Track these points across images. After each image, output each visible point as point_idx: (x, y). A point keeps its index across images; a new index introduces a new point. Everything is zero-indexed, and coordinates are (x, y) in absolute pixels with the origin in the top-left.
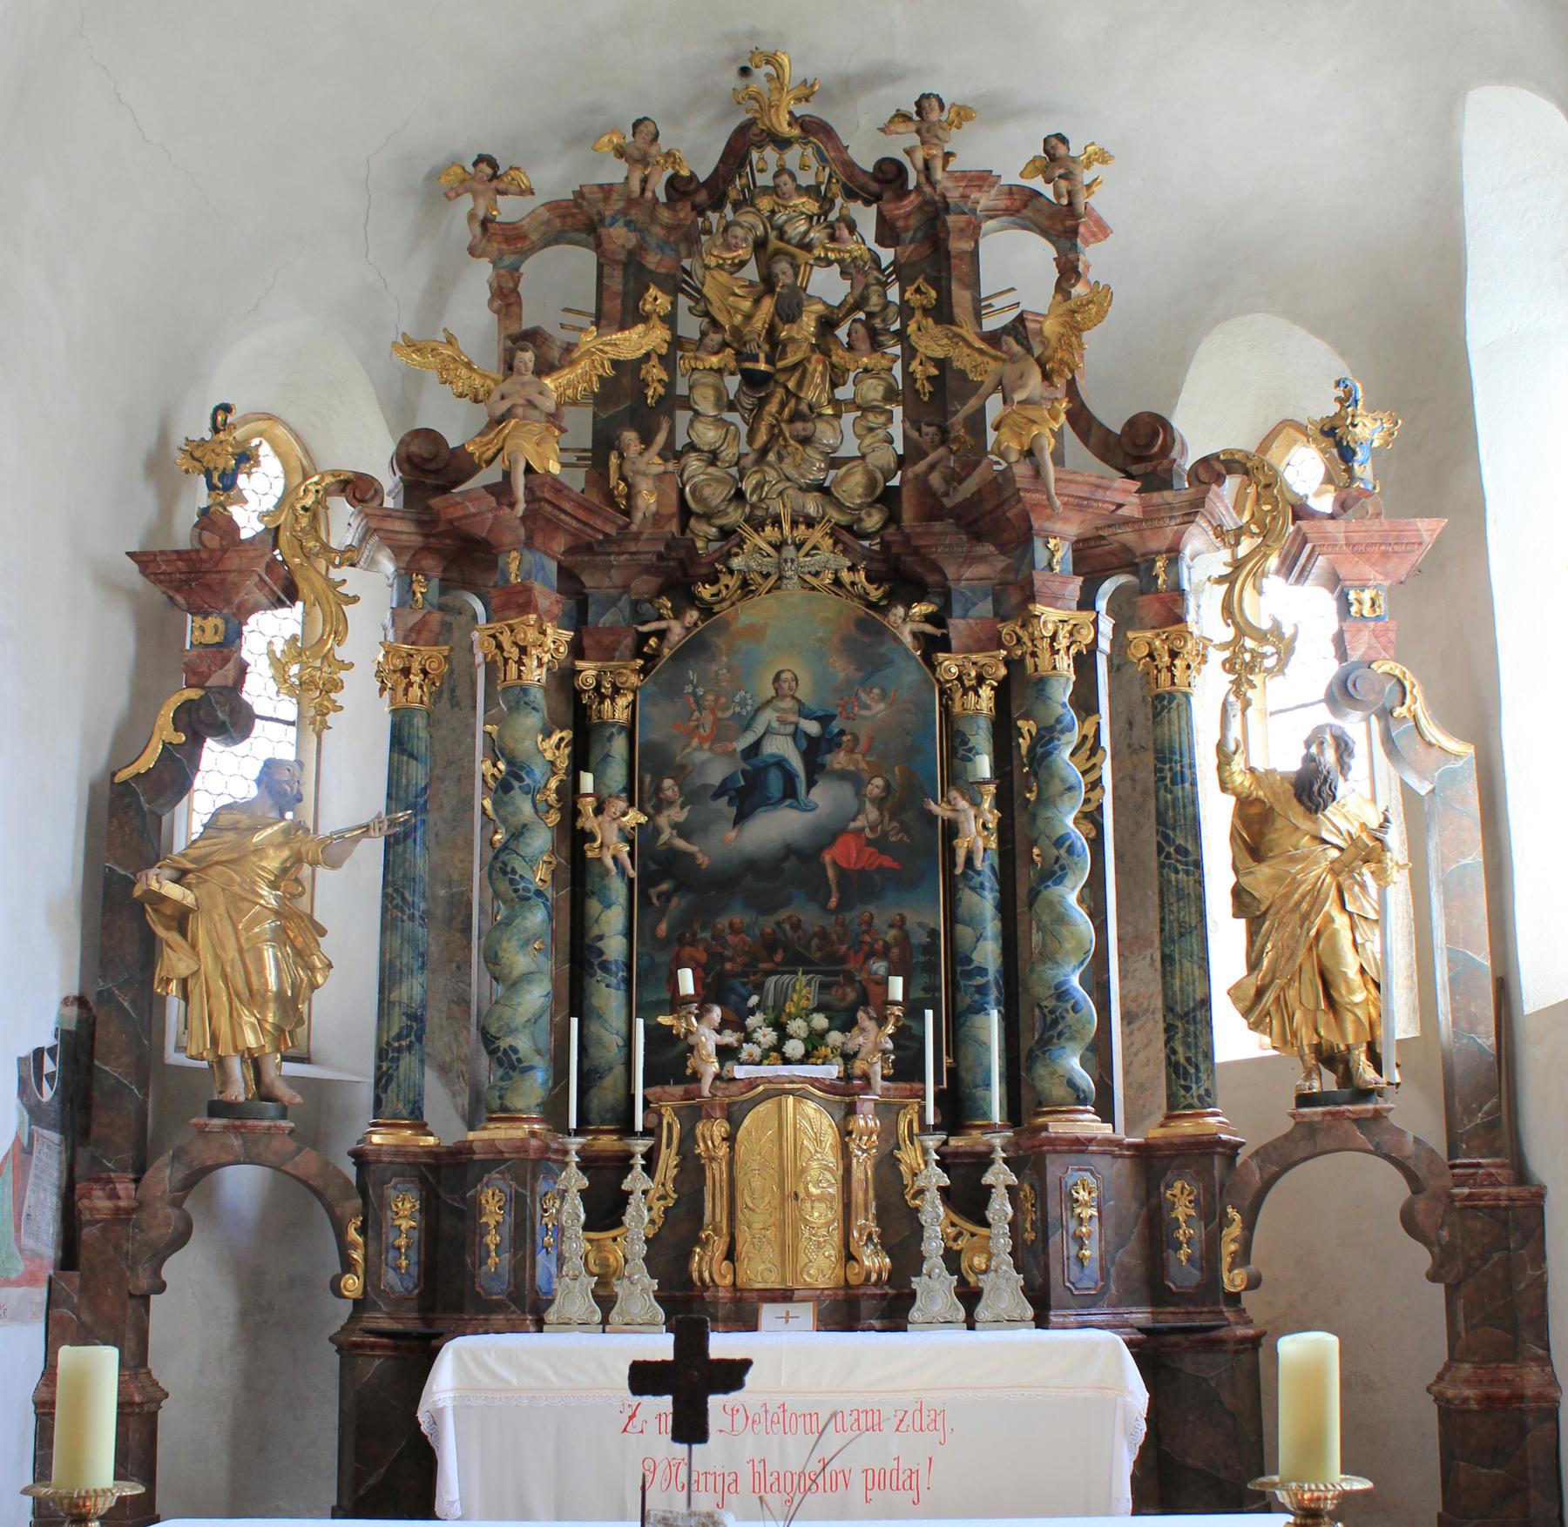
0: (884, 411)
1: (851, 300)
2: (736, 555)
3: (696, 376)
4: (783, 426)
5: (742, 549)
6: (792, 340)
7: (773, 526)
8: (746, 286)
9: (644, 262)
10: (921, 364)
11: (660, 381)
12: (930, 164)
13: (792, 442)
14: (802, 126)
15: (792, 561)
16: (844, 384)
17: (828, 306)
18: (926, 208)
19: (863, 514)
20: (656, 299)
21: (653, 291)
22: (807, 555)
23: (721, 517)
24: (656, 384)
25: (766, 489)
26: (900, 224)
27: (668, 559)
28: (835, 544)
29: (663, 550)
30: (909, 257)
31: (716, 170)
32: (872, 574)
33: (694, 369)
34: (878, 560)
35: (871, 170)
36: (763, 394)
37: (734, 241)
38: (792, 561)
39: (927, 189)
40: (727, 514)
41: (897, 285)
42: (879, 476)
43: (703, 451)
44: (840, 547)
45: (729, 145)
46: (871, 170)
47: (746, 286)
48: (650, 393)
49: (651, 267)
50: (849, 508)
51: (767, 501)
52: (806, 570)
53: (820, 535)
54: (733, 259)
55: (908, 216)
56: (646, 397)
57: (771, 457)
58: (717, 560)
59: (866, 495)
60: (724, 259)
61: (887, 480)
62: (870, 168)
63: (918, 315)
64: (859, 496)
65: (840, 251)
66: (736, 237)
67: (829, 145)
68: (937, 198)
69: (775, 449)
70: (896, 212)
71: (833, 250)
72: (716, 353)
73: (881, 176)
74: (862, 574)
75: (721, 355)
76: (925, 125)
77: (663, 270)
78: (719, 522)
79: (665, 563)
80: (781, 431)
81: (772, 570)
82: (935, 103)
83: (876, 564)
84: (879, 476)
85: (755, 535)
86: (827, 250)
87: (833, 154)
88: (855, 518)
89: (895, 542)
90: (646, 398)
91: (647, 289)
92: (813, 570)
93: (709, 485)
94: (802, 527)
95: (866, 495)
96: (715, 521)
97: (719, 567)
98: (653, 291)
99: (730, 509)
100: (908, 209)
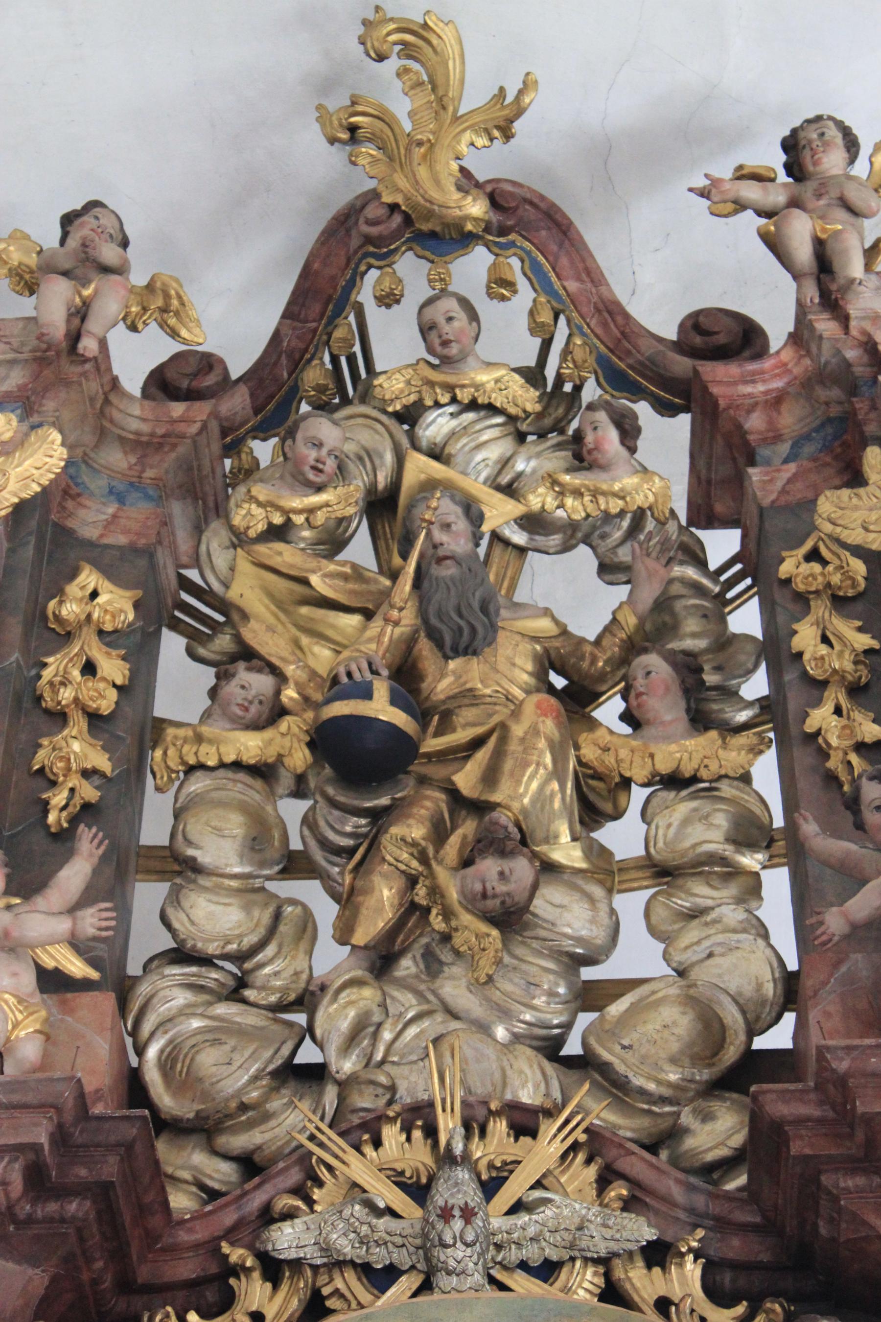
0: (733, 872)
1: (630, 621)
2: (289, 1215)
3: (198, 784)
4: (443, 875)
5: (310, 1202)
6: (469, 697)
7: (407, 1129)
8: (345, 577)
9: (70, 523)
10: (838, 711)
11: (87, 774)
12: (830, 247)
13: (466, 918)
14: (495, 201)
15: (468, 1214)
16: (617, 815)
17: (564, 632)
18: (822, 393)
19: (687, 1118)
20: (94, 595)
21: (89, 578)
22: (517, 1208)
23: (251, 1125)
24: (74, 781)
25: (387, 1036)
26: (755, 423)
27: (63, 1192)
28: (603, 1182)
29: (43, 1139)
30: (783, 491)
31: (276, 337)
32: (726, 1278)
33: (190, 770)
34: (744, 1228)
35: (673, 337)
36: (384, 801)
37: (312, 455)
38: (468, 1214)
39: (826, 325)
40: (267, 1117)
41: (754, 604)
42: (732, 1016)
43: (206, 961)
44: (619, 1190)
45: (306, 273)
46: (673, 337)
47: (345, 577)
48: (58, 798)
49: (90, 533)
50: (642, 1093)
51: (387, 1067)
52: (513, 1255)
53: (557, 1148)
54: (311, 511)
55: (777, 401)
56: (45, 807)
57: (407, 966)
58: (231, 1234)
59: (697, 1060)
60: (285, 512)
61: (752, 1032)
62: (671, 334)
63: (821, 608)
64: (673, 1061)
65: (595, 493)
66: (319, 445)
67: (564, 261)
68: (851, 354)
69: (417, 950)
70: (748, 389)
71: (578, 493)
72: (256, 726)
73: (698, 340)
74: (693, 1269)
75: (268, 733)
76: (810, 187)
77: (122, 540)
78: (239, 1142)
79: (52, 1207)
80: (435, 891)
81: (402, 1258)
82: (833, 133)
83: (736, 1242)
84: (732, 1016)
85: (351, 1156)
86: (562, 491)
87: (572, 286)
88: (665, 1124)
89: (800, 1121)
90: (46, 812)
91: (73, 574)
92: (533, 1254)
93: (216, 1042)
94: (500, 1127)
95: (697, 1060)
96: (226, 1141)
97: (236, 1254)
98: (89, 578)
99: (274, 1105)
100: (778, 384)
